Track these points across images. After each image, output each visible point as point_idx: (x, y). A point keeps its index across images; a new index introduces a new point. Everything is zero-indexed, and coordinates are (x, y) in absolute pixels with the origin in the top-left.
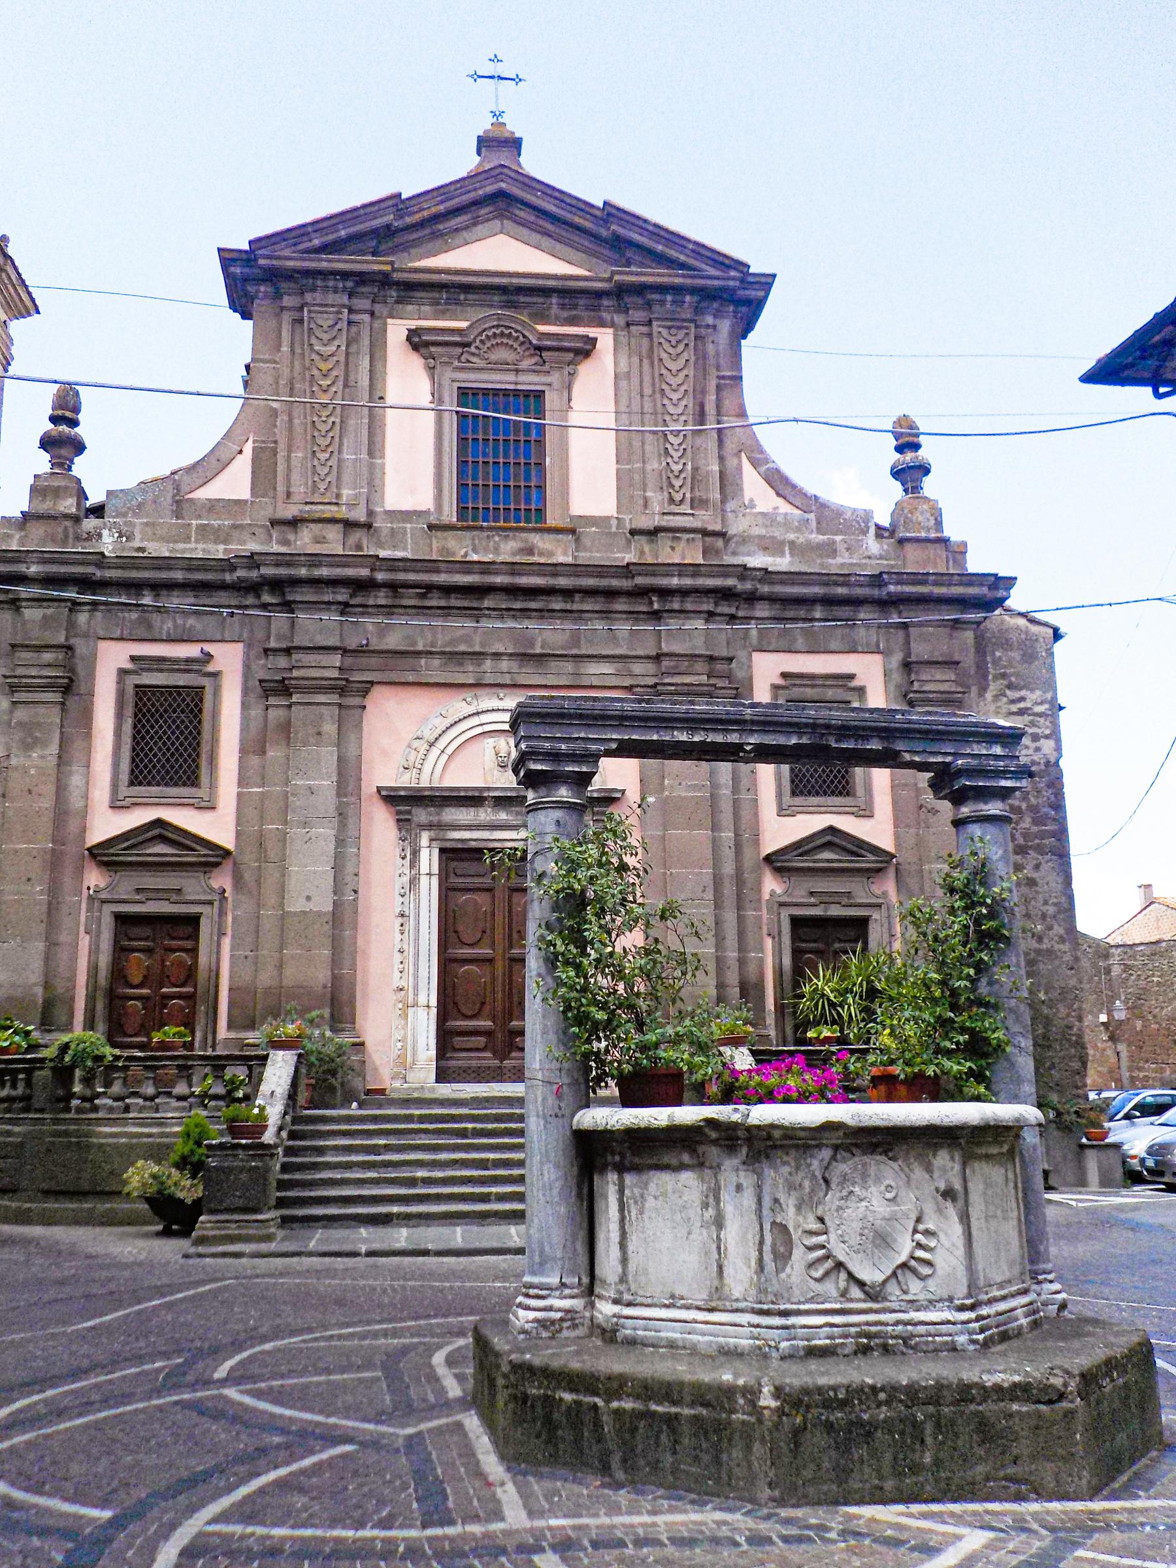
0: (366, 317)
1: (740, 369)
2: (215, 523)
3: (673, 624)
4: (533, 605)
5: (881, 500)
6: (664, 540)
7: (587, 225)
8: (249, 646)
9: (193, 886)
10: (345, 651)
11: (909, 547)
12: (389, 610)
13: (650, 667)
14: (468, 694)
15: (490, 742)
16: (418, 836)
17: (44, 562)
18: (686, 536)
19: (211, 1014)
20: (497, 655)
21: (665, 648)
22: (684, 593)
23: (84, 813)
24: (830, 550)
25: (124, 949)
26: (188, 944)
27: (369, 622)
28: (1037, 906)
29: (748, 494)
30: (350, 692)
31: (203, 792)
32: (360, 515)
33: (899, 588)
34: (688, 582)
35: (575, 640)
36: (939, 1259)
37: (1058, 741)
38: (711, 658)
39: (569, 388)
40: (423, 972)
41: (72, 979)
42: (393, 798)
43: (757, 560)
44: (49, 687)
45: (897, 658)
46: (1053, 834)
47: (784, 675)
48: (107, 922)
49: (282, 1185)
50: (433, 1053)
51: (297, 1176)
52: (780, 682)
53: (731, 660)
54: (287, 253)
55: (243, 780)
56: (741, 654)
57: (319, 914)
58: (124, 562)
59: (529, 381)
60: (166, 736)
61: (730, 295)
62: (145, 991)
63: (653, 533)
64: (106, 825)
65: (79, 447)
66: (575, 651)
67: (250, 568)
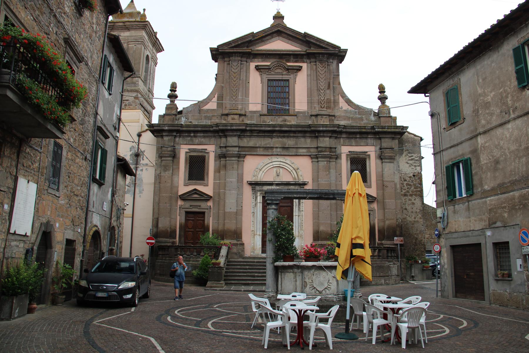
0: (245, 62)
2: (208, 115)
3: (321, 139)
4: (286, 135)
5: (375, 105)
6: (319, 117)
8: (216, 146)
9: (203, 205)
10: (239, 147)
11: (381, 118)
12: (250, 136)
13: (315, 150)
14: (270, 157)
15: (275, 169)
16: (257, 193)
18: (324, 117)
19: (243, 149)
20: (277, 147)
21: (319, 145)
22: (324, 131)
23: (178, 187)
26: (203, 219)
28: (415, 209)
29: (340, 105)
30: (240, 157)
31: (205, 182)
32: (243, 112)
33: (378, 130)
34: (325, 129)
35: (296, 144)
36: (332, 287)
37: (421, 167)
38: (331, 148)
39: (295, 79)
40: (258, 227)
41: (176, 225)
42: (251, 184)
43: (343, 123)
44: (170, 156)
45: (378, 147)
46: (419, 191)
49: (225, 276)
50: (261, 246)
51: (228, 274)
54: (226, 48)
55: (215, 179)
56: (338, 147)
58: (187, 126)
59: (285, 77)
60: (197, 168)
61: (338, 55)
63: (316, 116)
64: (183, 190)
65: (176, 97)
66: (296, 146)
67: (216, 127)
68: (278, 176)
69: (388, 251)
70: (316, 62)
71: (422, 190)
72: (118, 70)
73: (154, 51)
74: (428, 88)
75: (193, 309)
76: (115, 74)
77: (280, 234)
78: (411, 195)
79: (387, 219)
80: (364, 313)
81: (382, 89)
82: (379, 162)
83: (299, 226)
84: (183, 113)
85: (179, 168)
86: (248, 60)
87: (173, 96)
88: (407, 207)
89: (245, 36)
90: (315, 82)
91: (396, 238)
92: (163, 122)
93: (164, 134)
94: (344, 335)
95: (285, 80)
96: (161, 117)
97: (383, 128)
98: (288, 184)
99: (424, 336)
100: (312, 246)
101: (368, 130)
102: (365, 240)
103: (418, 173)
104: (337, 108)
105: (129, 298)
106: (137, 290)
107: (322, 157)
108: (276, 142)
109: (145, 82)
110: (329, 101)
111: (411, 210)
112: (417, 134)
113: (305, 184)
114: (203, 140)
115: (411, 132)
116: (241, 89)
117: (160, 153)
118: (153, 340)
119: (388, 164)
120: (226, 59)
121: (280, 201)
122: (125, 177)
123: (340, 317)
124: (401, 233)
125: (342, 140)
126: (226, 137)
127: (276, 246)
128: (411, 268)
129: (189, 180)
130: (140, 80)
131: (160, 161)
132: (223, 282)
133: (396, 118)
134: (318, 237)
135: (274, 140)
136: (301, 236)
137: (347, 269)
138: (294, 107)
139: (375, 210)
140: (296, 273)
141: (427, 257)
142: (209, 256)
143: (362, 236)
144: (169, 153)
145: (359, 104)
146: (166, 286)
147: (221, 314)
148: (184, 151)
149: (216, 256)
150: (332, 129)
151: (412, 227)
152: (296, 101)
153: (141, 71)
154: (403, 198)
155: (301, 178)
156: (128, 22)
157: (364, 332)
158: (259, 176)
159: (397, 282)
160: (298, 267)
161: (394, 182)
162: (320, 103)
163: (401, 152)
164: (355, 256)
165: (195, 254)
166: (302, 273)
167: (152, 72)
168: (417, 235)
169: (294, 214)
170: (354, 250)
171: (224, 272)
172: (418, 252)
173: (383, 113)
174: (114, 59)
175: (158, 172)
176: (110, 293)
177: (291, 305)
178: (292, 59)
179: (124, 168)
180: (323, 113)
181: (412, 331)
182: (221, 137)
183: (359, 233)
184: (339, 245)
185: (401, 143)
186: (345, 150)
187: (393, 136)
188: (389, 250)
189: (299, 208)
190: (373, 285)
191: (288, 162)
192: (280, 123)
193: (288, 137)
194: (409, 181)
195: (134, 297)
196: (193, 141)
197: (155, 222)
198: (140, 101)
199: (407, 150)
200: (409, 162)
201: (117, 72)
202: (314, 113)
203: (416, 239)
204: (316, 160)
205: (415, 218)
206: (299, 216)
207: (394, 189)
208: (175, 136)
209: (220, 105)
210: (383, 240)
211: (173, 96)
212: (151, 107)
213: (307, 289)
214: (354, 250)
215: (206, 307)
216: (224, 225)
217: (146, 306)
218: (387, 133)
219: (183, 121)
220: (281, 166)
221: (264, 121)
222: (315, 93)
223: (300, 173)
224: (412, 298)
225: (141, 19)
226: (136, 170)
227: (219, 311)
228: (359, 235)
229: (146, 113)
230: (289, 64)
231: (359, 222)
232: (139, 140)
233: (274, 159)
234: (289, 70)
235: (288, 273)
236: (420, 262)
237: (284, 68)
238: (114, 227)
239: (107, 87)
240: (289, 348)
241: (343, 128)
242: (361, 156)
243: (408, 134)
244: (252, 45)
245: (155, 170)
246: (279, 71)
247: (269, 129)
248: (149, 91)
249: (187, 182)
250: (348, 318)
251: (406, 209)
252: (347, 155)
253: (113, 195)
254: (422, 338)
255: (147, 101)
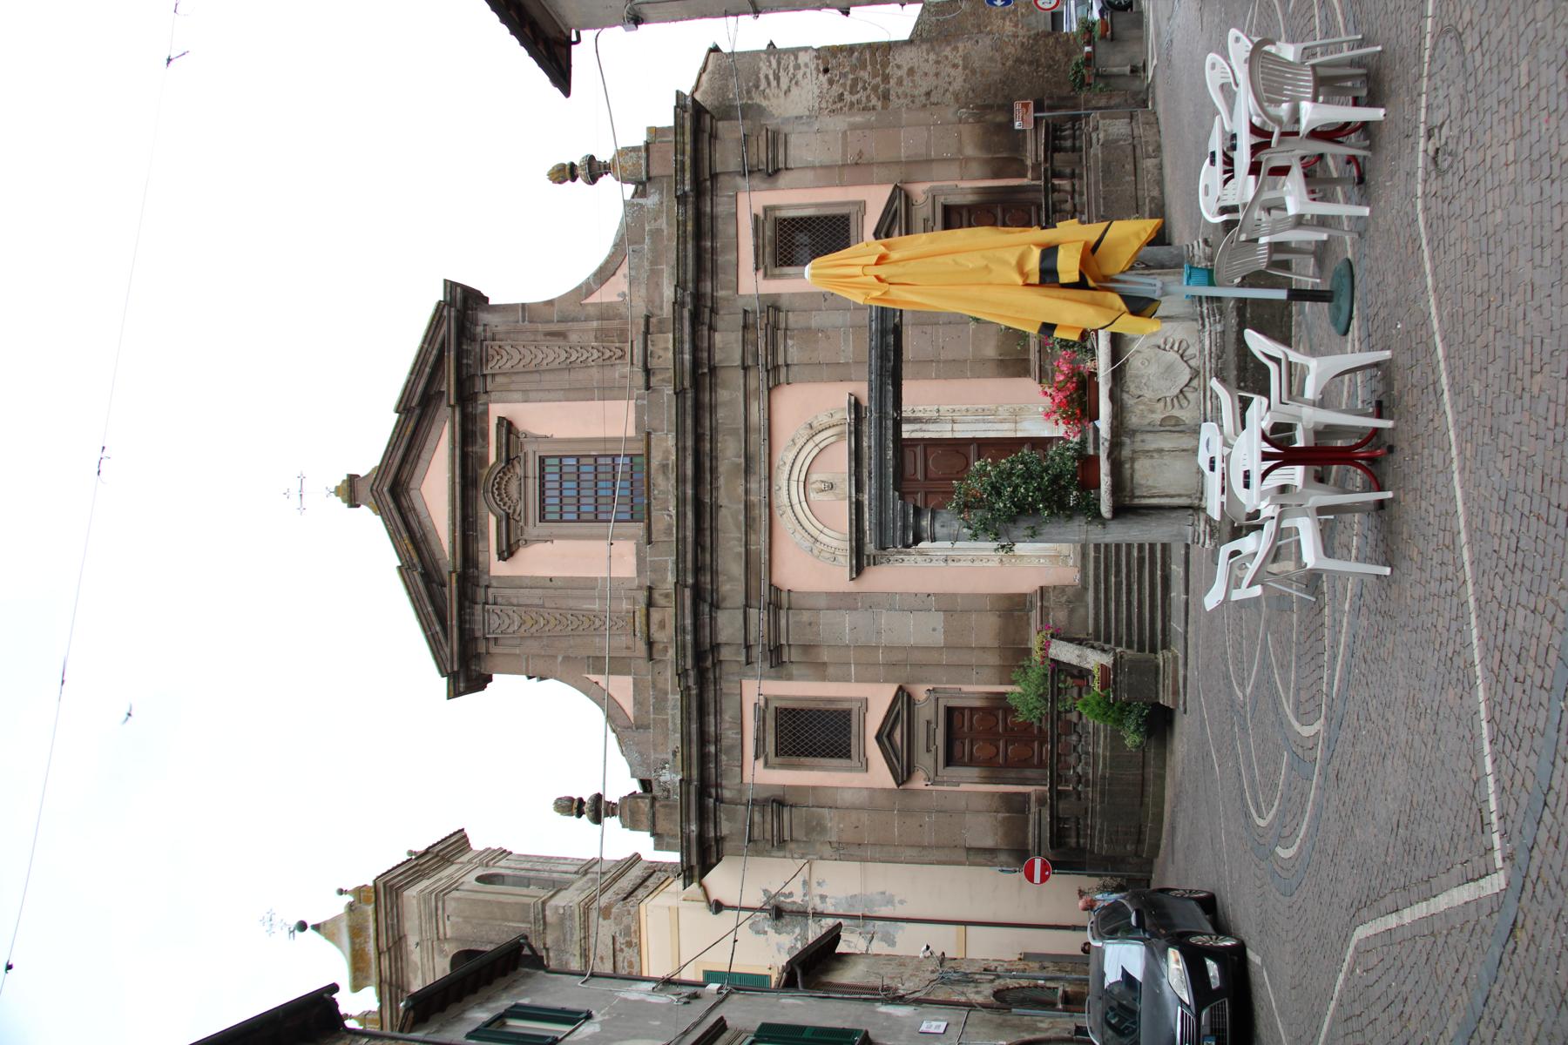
0: (490, 591)
1: (516, 305)
2: (652, 701)
3: (718, 357)
4: (708, 465)
5: (613, 194)
6: (653, 363)
7: (412, 424)
8: (745, 675)
9: (924, 712)
10: (747, 606)
11: (652, 174)
12: (714, 573)
13: (752, 374)
14: (777, 513)
15: (813, 496)
17: (688, 821)
18: (650, 348)
19: (753, 593)
20: (747, 492)
21: (738, 362)
22: (695, 349)
23: (872, 790)
24: (656, 233)
25: (971, 758)
26: (967, 713)
27: (725, 588)
30: (777, 602)
31: (855, 707)
32: (642, 596)
33: (687, 182)
34: (687, 347)
36: (1178, 337)
38: (745, 327)
41: (987, 794)
42: (858, 569)
43: (668, 292)
45: (739, 180)
46: (873, 55)
47: (757, 269)
48: (952, 771)
51: (1135, 638)
52: (761, 273)
53: (745, 312)
54: (448, 651)
56: (741, 304)
57: (946, 621)
59: (533, 468)
60: (812, 733)
61: (462, 309)
62: (1001, 744)
63: (648, 372)
64: (879, 774)
65: (598, 798)
68: (832, 487)
69: (1057, 149)
70: (485, 376)
71: (870, 46)
72: (515, 991)
73: (465, 858)
74: (552, 33)
75: (1250, 766)
76: (525, 1001)
77: (1013, 503)
78: (886, 79)
79: (960, 151)
80: (1263, 240)
81: (565, 173)
82: (784, 179)
83: (984, 421)
84: (646, 777)
85: (814, 788)
86: (483, 582)
87: (597, 809)
88: (923, 90)
89: (409, 593)
90: (547, 377)
91: (1017, 125)
92: (674, 836)
93: (712, 834)
94: (1339, 308)
95: (542, 469)
96: (661, 842)
97: (680, 168)
98: (857, 456)
99: (1338, 47)
100: (1042, 377)
101: (690, 213)
102: (1025, 242)
103: (818, 58)
104: (622, 310)
105: (1222, 970)
106: (1193, 940)
107: (774, 354)
108: (729, 496)
109: (558, 886)
110: (602, 335)
111: (931, 78)
112: (700, 64)
113: (856, 406)
114: (727, 717)
115: (693, 82)
116: (571, 603)
117: (769, 847)
118: (1361, 932)
119: (792, 152)
120: (482, 649)
121: (909, 484)
122: (843, 957)
123: (1276, 324)
124: (1000, 108)
125: (721, 293)
126: (718, 645)
127: (1052, 514)
128: (1107, 77)
129: (849, 757)
130: (553, 902)
131: (792, 846)
132: (1160, 656)
133: (650, 130)
134: (1016, 360)
135: (723, 501)
136: (1015, 416)
137: (1126, 299)
138: (617, 440)
139: (932, 189)
140: (1134, 452)
141: (1075, 28)
142: (1080, 695)
143: (1017, 252)
144: (769, 818)
145: (611, 243)
146: (1173, 828)
147: (1265, 682)
148: (761, 775)
149: (1082, 674)
150: (687, 324)
151: (983, 74)
152: (601, 435)
153: (526, 900)
154: (895, 102)
155: (838, 417)
156: (377, 939)
157: (1324, 237)
158: (835, 544)
159: (1152, 119)
160: (1116, 445)
161: (845, 133)
162: (606, 363)
163: (751, 111)
164: (1082, 275)
165: (1074, 738)
166: (1133, 433)
167: (528, 866)
168: (1005, 58)
169: (949, 435)
170: (1063, 279)
171: (1130, 654)
172: (1059, 56)
173: (638, 168)
174: (480, 1005)
175: (827, 850)
176: (1206, 1030)
177: (1247, 485)
178: (477, 448)
179: (815, 966)
180: (638, 351)
181: (1327, 85)
182: (718, 663)
183: (1005, 263)
184: (1048, 328)
185: (726, 112)
186: (750, 282)
187: (706, 136)
188: (1053, 146)
189: (929, 421)
190: (1162, 193)
191: (791, 456)
192: (673, 481)
193: (714, 458)
194: (844, 85)
195: (1216, 954)
196: (732, 747)
197: (979, 859)
198: (617, 901)
199: (748, 92)
200: (784, 86)
201: (521, 995)
202: (640, 379)
203: (1018, 60)
204: (783, 371)
205: (955, 66)
206: (954, 422)
207: (867, 132)
208: (719, 799)
209: (619, 666)
210: (1022, 162)
211: (597, 809)
212: (632, 865)
213: (1186, 415)
214: (1063, 279)
215: (1244, 729)
216: (983, 648)
217: (1248, 914)
218: (700, 151)
219: (670, 777)
220: (802, 478)
221: (668, 532)
222: (580, 376)
223: (825, 420)
224: (1213, 80)
225: (367, 902)
226: (823, 915)
227: (1257, 687)
228: (1013, 261)
229: (651, 883)
230: (492, 459)
231: (972, 262)
232: (734, 908)
233: (781, 498)
234: (510, 457)
235: (1137, 476)
236: (1088, 49)
237: (504, 471)
238: (997, 994)
239: (568, 1028)
240: (1389, 495)
241: (685, 290)
242: (769, 233)
243: (701, 89)
244: (438, 570)
245: (822, 858)
246: (513, 488)
247: (690, 515)
248: (586, 873)
249: (855, 762)
250: (1282, 294)
251: (928, 94)
252: (765, 276)
253: (900, 1000)
254: (1347, 53)
255: (615, 880)
